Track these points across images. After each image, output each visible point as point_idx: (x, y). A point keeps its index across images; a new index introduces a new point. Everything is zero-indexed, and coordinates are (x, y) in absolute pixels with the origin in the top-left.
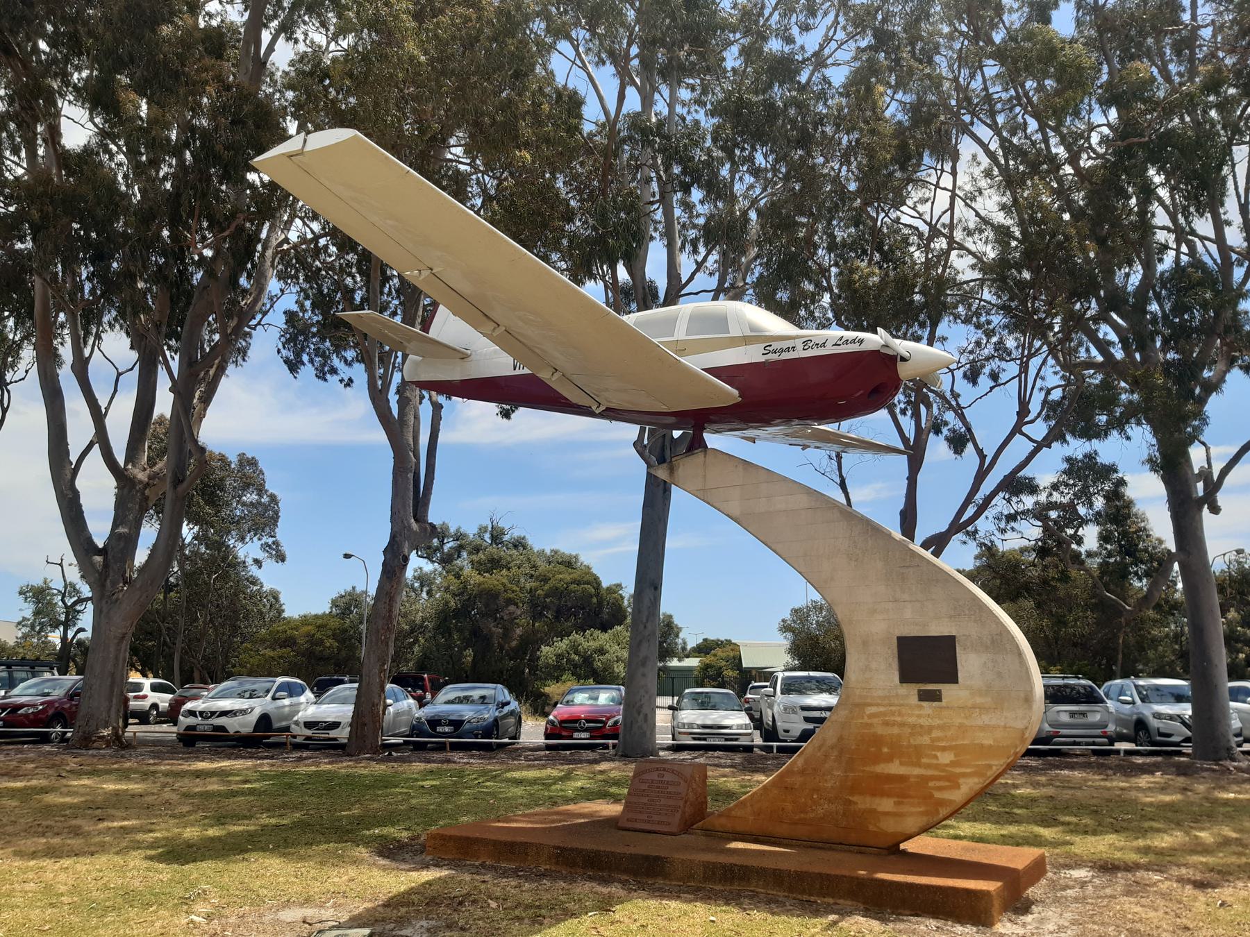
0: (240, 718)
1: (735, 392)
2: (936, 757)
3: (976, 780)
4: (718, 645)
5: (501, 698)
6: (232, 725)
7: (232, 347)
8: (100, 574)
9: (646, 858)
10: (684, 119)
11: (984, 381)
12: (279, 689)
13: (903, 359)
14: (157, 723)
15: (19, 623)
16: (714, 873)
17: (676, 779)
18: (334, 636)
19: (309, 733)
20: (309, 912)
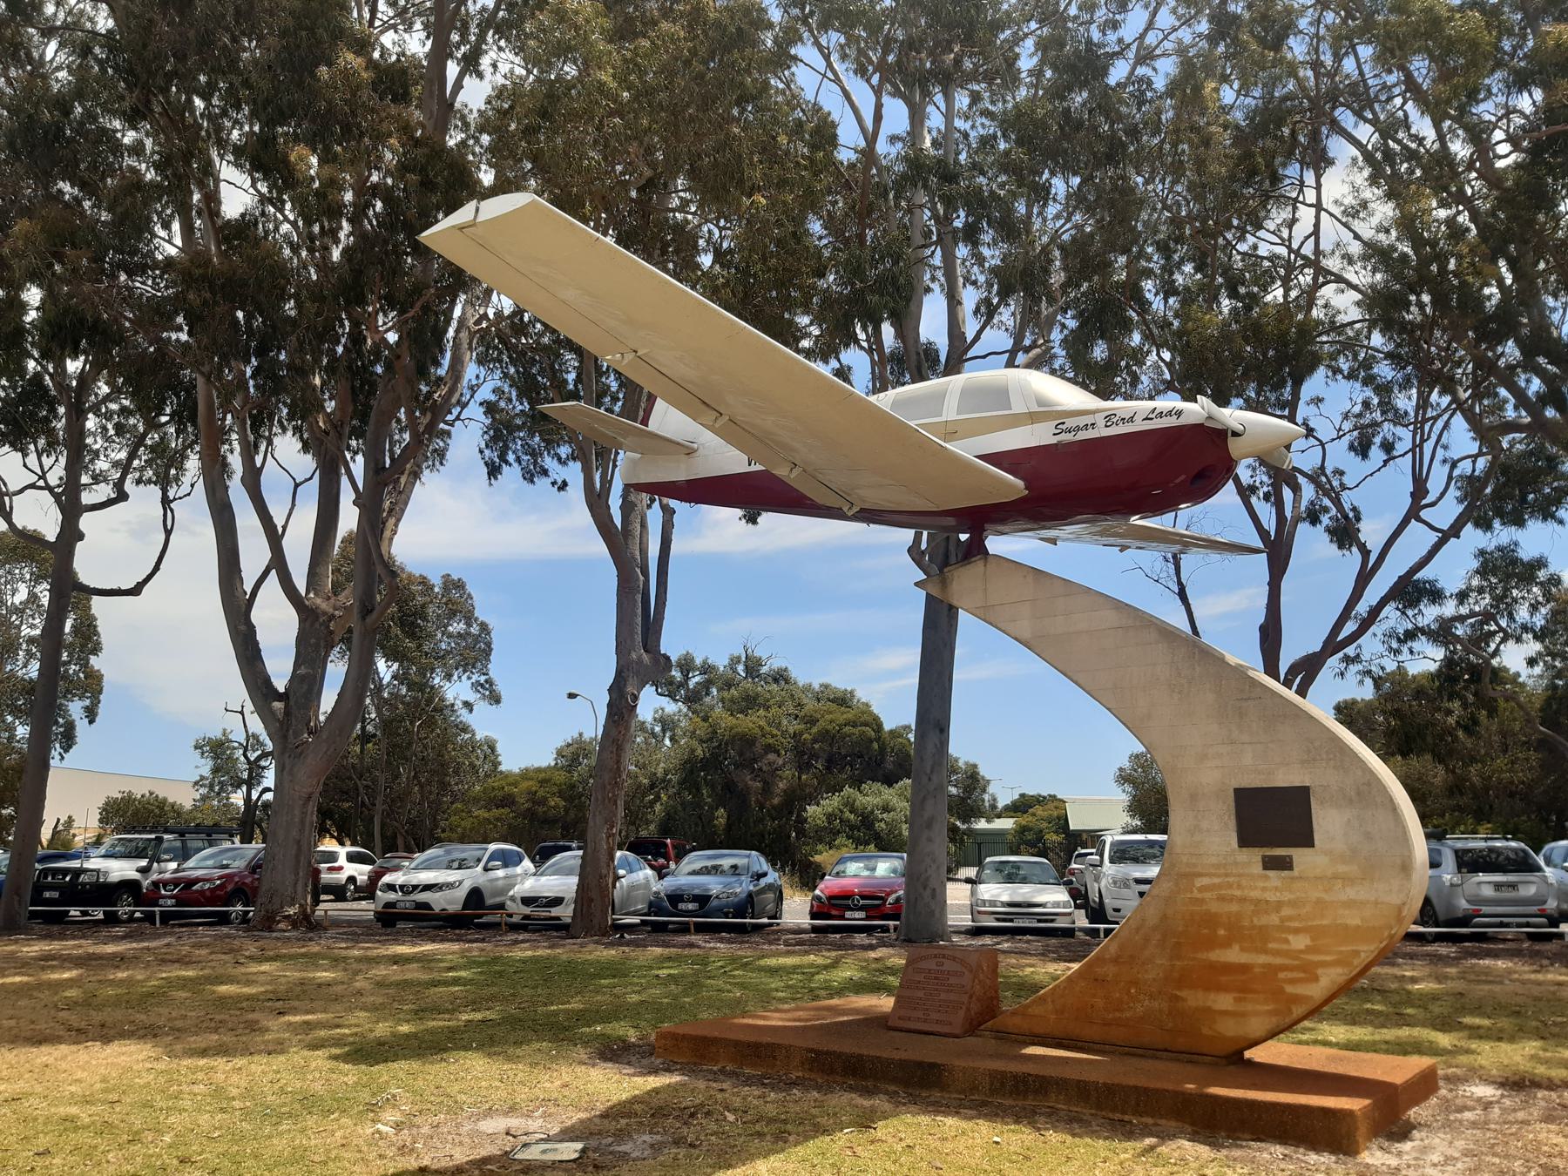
0: (447, 893)
1: (1020, 483)
2: (1287, 941)
3: (1339, 970)
4: (1039, 802)
5: (756, 868)
6: (437, 900)
7: (426, 446)
8: (281, 723)
9: (920, 1064)
10: (966, 135)
11: (1377, 454)
12: (492, 858)
13: (1235, 434)
14: (355, 899)
15: (196, 783)
16: (1003, 1084)
17: (956, 967)
18: (561, 794)
19: (527, 910)
20: (514, 1122)
